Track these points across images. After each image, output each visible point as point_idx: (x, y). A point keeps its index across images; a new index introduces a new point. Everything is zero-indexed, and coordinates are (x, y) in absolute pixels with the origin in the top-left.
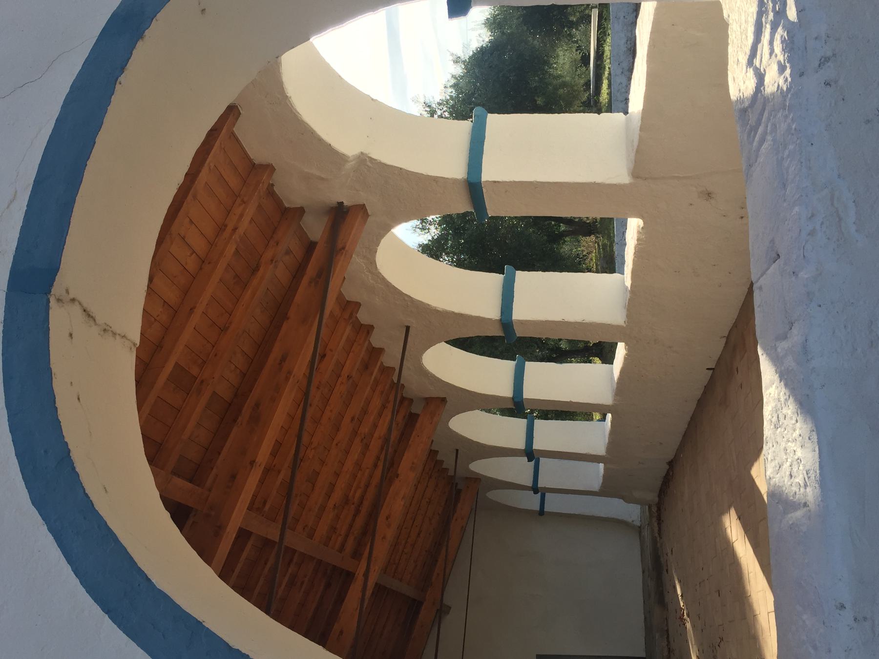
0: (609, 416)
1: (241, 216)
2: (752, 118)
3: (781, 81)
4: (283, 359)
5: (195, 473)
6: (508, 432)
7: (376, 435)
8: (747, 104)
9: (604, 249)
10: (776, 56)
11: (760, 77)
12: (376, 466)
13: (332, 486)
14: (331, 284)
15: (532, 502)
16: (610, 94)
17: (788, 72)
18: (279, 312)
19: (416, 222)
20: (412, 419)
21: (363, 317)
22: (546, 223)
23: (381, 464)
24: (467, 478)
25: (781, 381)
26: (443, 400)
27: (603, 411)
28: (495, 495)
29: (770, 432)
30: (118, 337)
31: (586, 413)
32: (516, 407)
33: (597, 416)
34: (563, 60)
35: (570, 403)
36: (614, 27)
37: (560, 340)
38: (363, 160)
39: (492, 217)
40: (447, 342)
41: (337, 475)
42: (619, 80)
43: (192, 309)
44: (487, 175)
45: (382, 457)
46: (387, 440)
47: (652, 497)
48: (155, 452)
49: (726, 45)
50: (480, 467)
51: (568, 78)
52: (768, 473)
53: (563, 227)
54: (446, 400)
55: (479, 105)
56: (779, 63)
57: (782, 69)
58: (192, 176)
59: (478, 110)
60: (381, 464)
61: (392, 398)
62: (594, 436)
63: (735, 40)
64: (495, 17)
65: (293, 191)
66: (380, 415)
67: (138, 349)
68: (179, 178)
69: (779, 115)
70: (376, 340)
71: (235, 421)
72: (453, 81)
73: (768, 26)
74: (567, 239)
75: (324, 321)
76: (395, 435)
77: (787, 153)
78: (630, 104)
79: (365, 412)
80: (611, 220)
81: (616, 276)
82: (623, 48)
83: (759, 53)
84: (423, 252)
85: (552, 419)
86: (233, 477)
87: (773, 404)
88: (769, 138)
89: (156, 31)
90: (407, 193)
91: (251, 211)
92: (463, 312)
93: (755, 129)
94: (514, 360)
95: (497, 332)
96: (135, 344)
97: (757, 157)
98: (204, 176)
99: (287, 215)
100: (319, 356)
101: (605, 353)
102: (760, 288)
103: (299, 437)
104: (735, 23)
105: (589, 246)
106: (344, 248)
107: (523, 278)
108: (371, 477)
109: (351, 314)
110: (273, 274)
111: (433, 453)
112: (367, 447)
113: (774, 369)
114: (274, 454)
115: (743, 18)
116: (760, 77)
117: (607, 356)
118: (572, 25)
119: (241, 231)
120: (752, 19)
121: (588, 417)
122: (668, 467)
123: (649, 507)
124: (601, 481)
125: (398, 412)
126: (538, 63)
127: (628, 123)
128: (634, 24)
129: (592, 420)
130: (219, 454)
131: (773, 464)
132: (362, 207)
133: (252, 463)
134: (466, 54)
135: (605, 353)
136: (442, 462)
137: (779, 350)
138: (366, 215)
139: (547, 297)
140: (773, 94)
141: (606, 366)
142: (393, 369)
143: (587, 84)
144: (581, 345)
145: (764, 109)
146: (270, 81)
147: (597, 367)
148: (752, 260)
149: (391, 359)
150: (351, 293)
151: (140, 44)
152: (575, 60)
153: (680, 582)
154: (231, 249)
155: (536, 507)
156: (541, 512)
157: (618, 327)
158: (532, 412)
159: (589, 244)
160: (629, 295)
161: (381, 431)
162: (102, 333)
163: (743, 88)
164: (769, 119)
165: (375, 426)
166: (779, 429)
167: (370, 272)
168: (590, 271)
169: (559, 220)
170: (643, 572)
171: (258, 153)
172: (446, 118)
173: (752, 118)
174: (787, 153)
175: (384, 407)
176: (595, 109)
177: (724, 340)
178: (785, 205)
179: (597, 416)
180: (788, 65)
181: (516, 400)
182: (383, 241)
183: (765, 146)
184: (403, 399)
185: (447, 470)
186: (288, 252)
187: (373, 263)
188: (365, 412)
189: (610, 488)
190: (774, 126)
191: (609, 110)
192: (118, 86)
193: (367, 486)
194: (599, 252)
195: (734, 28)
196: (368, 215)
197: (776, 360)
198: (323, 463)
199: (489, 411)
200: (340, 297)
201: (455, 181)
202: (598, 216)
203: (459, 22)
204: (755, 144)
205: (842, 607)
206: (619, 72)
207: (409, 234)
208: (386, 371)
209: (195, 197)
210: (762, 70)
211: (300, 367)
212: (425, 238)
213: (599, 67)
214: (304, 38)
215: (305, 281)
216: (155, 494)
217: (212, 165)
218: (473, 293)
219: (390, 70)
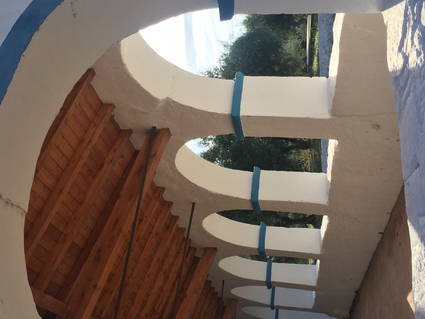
0: (318, 261)
1: (94, 134)
2: (402, 82)
3: (419, 62)
4: (117, 222)
5: (59, 293)
6: (255, 270)
7: (173, 270)
8: (398, 74)
9: (315, 158)
10: (415, 46)
11: (406, 58)
12: (172, 290)
13: (145, 302)
14: (147, 177)
16: (318, 65)
17: (422, 55)
18: (115, 192)
19: (200, 140)
20: (196, 261)
21: (166, 196)
22: (280, 141)
23: (175, 289)
25: (422, 242)
26: (215, 249)
27: (315, 258)
28: (247, 310)
29: (416, 273)
30: (15, 207)
31: (305, 259)
32: (260, 254)
33: (311, 261)
34: (290, 46)
35: (294, 253)
36: (320, 26)
37: (288, 213)
38: (169, 102)
39: (246, 137)
40: (218, 213)
41: (148, 295)
42: (322, 58)
43: (61, 190)
44: (244, 111)
45: (176, 284)
46: (179, 273)
48: (35, 278)
49: (386, 38)
50: (237, 292)
51: (293, 55)
52: (415, 299)
53: (290, 144)
54: (217, 249)
55: (238, 71)
56: (417, 50)
57: (419, 54)
58: (64, 110)
59: (238, 74)
60: (175, 289)
61: (183, 247)
62: (309, 274)
63: (391, 37)
64: (249, 19)
65: (125, 119)
66: (176, 258)
67: (27, 215)
68: (57, 111)
69: (418, 81)
70: (174, 211)
71: (85, 260)
72: (224, 57)
73: (410, 29)
74: (293, 151)
75: (142, 198)
76: (184, 271)
77: (422, 103)
78: (330, 72)
79: (166, 255)
80: (320, 140)
81: (322, 174)
82: (326, 38)
83: (405, 44)
84: (204, 158)
85: (283, 262)
86: (83, 295)
87: (418, 256)
88: (412, 94)
89: (46, 27)
90: (195, 122)
91: (100, 131)
92: (228, 195)
93: (403, 88)
94: (259, 225)
95: (250, 208)
96: (25, 211)
97: (405, 105)
98: (72, 110)
99: (123, 133)
100: (139, 220)
101: (315, 222)
102: (408, 184)
103: (125, 271)
104: (391, 27)
105: (306, 156)
106: (155, 154)
107: (264, 174)
108: (169, 297)
109: (159, 194)
110: (112, 169)
111: (208, 283)
112: (167, 277)
113: (417, 235)
114: (109, 281)
115: (396, 24)
116: (406, 58)
117: (317, 225)
118: (296, 24)
119: (93, 143)
120: (401, 26)
121: (306, 262)
122: (355, 294)
124: (313, 302)
125: (187, 256)
126: (276, 46)
127: (328, 83)
128: (332, 25)
129: (308, 263)
130: (75, 280)
131: (418, 294)
132: (167, 131)
133: (95, 286)
134: (231, 42)
135: (315, 222)
136: (214, 288)
137: (420, 223)
138: (169, 134)
139: (279, 186)
140: (413, 68)
141: (317, 230)
142: (184, 229)
143: (305, 59)
144: (301, 217)
145: (408, 78)
146: (114, 55)
147: (311, 230)
148: (403, 167)
149: (183, 223)
150: (159, 182)
151: (36, 33)
152: (298, 45)
154: (87, 154)
157: (324, 206)
158: (271, 257)
159: (306, 155)
160: (330, 186)
161: (176, 268)
162: (5, 204)
163: (396, 64)
164: (411, 83)
165: (172, 264)
166: (421, 272)
167: (171, 169)
168: (306, 171)
169: (288, 139)
171: (105, 96)
172: (220, 78)
173: (402, 82)
174: (422, 103)
175: (178, 253)
176: (309, 74)
177: (389, 216)
178: (422, 134)
179: (311, 261)
180: (422, 52)
181: (261, 250)
182: (179, 150)
183: (410, 98)
184: (190, 248)
185: (217, 293)
186: (122, 156)
187: (173, 164)
188: (166, 255)
190: (415, 87)
191: (318, 75)
192: (22, 57)
193: (167, 303)
194: (312, 160)
195: (391, 29)
196: (171, 135)
197: (418, 229)
198: (139, 287)
199: (243, 257)
200: (153, 183)
201: (223, 115)
202: (312, 138)
203: (226, 23)
204: (404, 97)
206: (324, 52)
207: (196, 147)
208: (180, 230)
209: (66, 123)
210: (407, 54)
211: (127, 227)
212: (206, 149)
213: (312, 49)
214: (136, 31)
215: (131, 173)
216: (33, 305)
217: (77, 104)
218: (234, 183)
219: (185, 51)
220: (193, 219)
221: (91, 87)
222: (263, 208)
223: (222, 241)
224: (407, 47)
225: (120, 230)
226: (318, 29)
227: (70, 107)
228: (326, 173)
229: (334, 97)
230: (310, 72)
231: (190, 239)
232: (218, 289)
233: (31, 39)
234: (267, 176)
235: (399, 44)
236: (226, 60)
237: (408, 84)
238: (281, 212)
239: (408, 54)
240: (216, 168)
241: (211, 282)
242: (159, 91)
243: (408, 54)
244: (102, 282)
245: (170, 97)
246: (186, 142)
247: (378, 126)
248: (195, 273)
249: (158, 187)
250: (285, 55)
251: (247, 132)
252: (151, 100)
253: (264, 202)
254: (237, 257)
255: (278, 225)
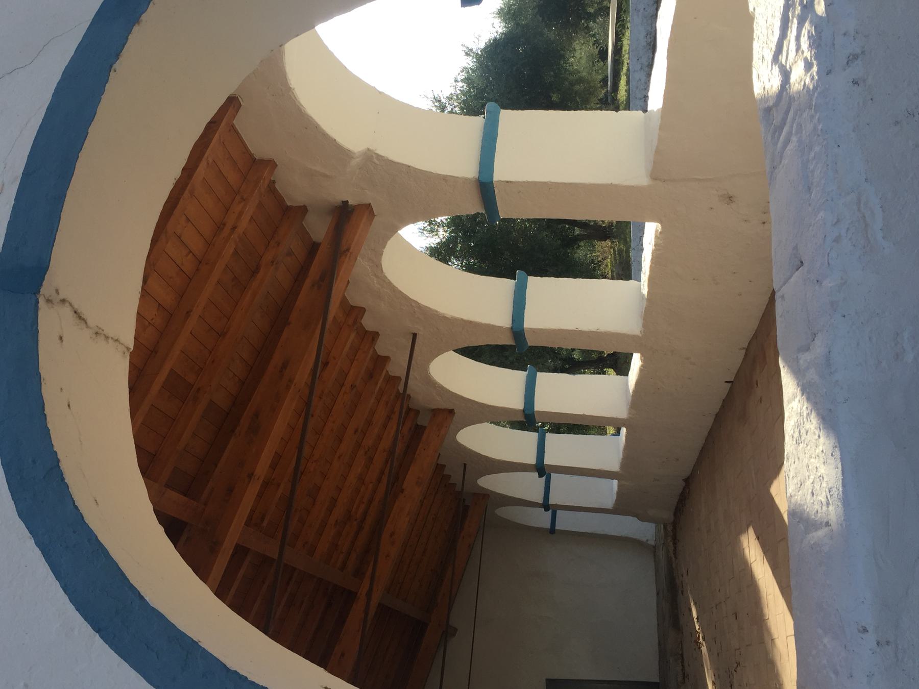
0: (624, 430)
2: (777, 117)
3: (808, 80)
4: (285, 366)
6: (518, 446)
8: (771, 103)
9: (619, 255)
10: (803, 52)
11: (786, 74)
12: (379, 480)
15: (542, 519)
16: (628, 91)
17: (815, 68)
18: (280, 315)
19: (421, 224)
20: (418, 431)
21: (368, 323)
22: (560, 226)
23: (385, 479)
24: (475, 494)
26: (451, 412)
28: (506, 512)
30: (110, 341)
33: (611, 430)
34: (580, 55)
35: (583, 417)
37: (573, 350)
38: (370, 157)
40: (454, 351)
42: (637, 76)
44: (499, 175)
45: (387, 471)
47: (668, 516)
49: (750, 39)
50: (488, 482)
51: (584, 74)
53: (577, 231)
54: (452, 412)
56: (806, 60)
57: (808, 66)
58: (189, 171)
59: (490, 106)
60: (385, 479)
62: (606, 452)
63: (761, 36)
65: (296, 188)
66: (385, 426)
69: (805, 115)
73: (795, 21)
74: (582, 244)
75: (327, 327)
81: (632, 283)
82: (643, 42)
83: (785, 49)
84: (431, 255)
88: (794, 139)
90: (416, 194)
93: (781, 128)
95: (508, 341)
96: (128, 349)
97: (781, 157)
98: (202, 170)
100: (322, 364)
103: (300, 450)
106: (348, 250)
107: (534, 283)
111: (440, 468)
114: (273, 466)
116: (786, 74)
121: (601, 431)
122: (683, 484)
123: (665, 527)
125: (403, 424)
128: (655, 16)
129: (606, 434)
133: (251, 475)
137: (801, 362)
138: (372, 214)
139: (561, 305)
140: (799, 92)
141: (621, 378)
142: (399, 378)
143: (605, 80)
144: (595, 356)
145: (787, 113)
147: (611, 378)
149: (397, 368)
150: (356, 298)
151: (136, 29)
153: (695, 604)
154: (229, 250)
155: (547, 525)
156: (552, 530)
158: (543, 425)
159: (604, 249)
160: (645, 303)
162: (94, 336)
163: (768, 86)
164: (794, 119)
165: (380, 438)
168: (605, 277)
169: (574, 223)
170: (658, 594)
171: (259, 147)
173: (777, 117)
174: (812, 154)
175: (389, 418)
177: (743, 352)
178: (810, 209)
179: (611, 430)
180: (815, 62)
181: (527, 412)
182: (389, 242)
184: (409, 410)
185: (454, 485)
187: (379, 266)
189: (622, 506)
190: (800, 126)
191: (628, 107)
192: (112, 73)
193: (370, 501)
194: (615, 258)
197: (797, 373)
200: (344, 301)
201: (465, 180)
204: (780, 145)
205: (865, 630)
206: (638, 67)
207: (417, 236)
208: (392, 380)
211: (302, 376)
212: (434, 241)
213: (617, 63)
216: (150, 507)
217: (211, 161)
218: (482, 299)
220: (413, 362)
221: (233, 129)
222: (531, 341)
223: (462, 397)
224: (787, 54)
225: (291, 381)
226: (629, 25)
227: (197, 167)
228: (640, 281)
229: (657, 147)
230: (613, 103)
231: (409, 396)
232: (456, 478)
233: (127, 39)
234: (540, 288)
235: (774, 49)
236: (467, 80)
237: (788, 120)
238: (562, 349)
239: (790, 68)
240: (453, 274)
241: (443, 466)
242: (351, 134)
243: (790, 68)
244: (262, 468)
245: (371, 148)
246: (400, 228)
247: (730, 199)
248: (417, 452)
249: (353, 307)
250: (571, 73)
251: (505, 210)
252: (340, 153)
253: (534, 331)
254: (486, 425)
255: (555, 370)
